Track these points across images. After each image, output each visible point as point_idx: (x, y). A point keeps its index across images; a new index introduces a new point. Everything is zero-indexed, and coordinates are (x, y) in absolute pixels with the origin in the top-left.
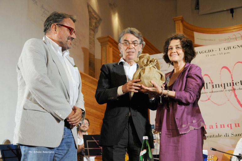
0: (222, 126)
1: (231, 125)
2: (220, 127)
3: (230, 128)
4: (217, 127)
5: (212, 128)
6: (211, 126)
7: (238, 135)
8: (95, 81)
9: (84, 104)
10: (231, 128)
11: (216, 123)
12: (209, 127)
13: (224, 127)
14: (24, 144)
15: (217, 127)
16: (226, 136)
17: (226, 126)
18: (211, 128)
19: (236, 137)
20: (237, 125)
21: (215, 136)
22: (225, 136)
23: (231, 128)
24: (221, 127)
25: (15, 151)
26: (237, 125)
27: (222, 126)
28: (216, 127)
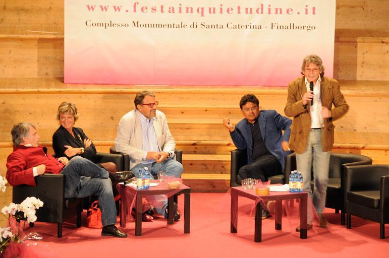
0: (189, 10)
1: (203, 9)
2: (219, 12)
3: (201, 14)
4: (180, 11)
5: (173, 12)
6: (171, 9)
7: (210, 27)
8: (336, 143)
9: (55, 242)
10: (203, 15)
11: (307, 6)
12: (169, 10)
13: (281, 13)
14: (277, 239)
15: (180, 11)
16: (192, 26)
17: (195, 10)
18: (171, 11)
19: (208, 29)
20: (190, 10)
21: (219, 27)
22: (191, 26)
23: (203, 15)
24: (276, 13)
25: (120, 214)
26: (190, 10)
27: (189, 10)
28: (268, 12)
